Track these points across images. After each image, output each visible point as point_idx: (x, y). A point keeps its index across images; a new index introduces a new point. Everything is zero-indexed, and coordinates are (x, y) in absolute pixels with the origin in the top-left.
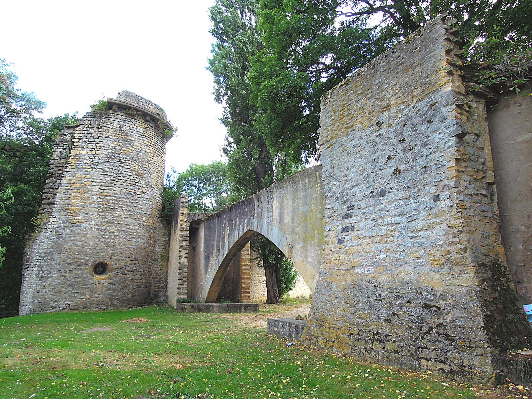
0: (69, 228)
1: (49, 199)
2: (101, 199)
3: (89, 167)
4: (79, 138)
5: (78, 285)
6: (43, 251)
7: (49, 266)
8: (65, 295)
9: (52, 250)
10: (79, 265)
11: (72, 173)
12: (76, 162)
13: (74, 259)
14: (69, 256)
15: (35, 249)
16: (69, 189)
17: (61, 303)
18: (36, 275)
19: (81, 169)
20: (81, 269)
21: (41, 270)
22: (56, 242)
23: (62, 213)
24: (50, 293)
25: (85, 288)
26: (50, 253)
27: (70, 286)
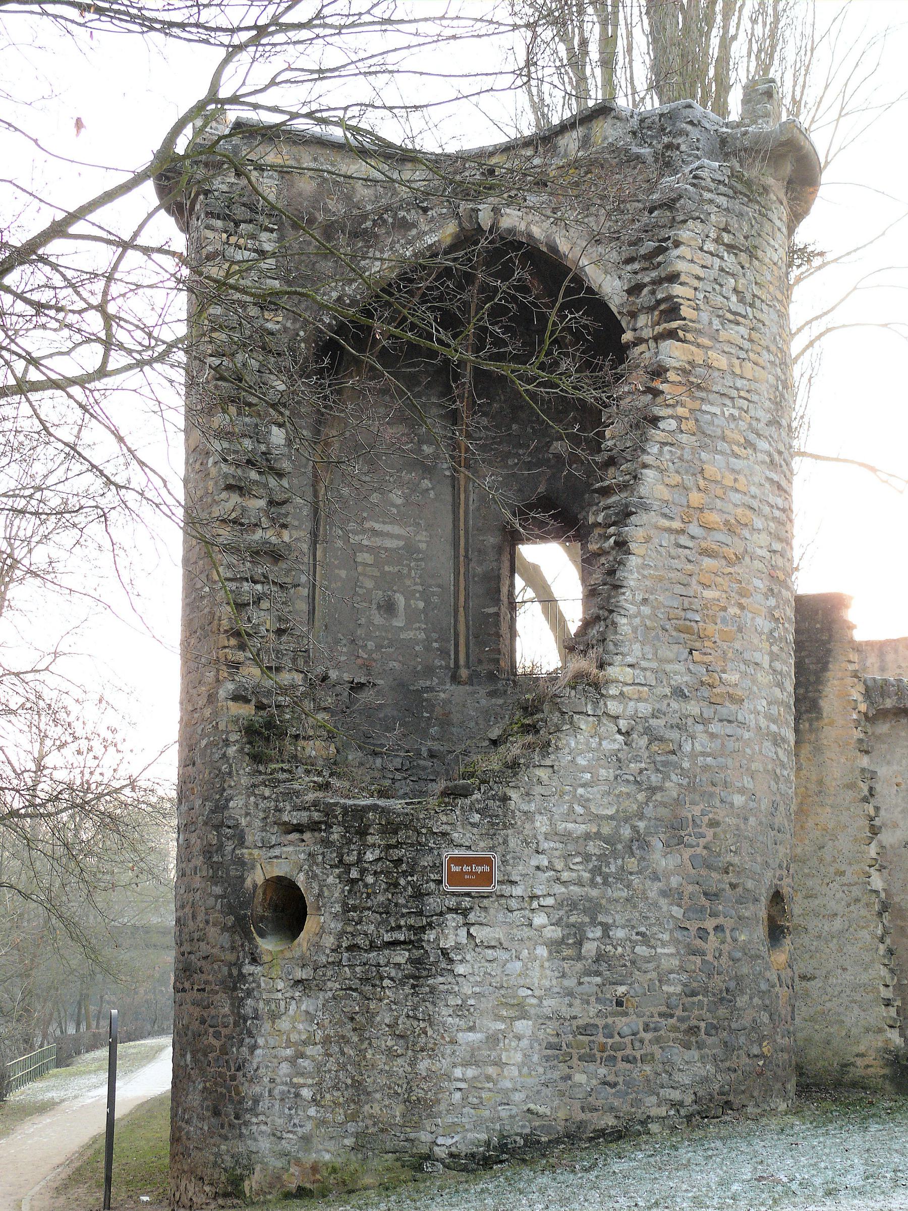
18: (555, 946)
21: (594, 922)
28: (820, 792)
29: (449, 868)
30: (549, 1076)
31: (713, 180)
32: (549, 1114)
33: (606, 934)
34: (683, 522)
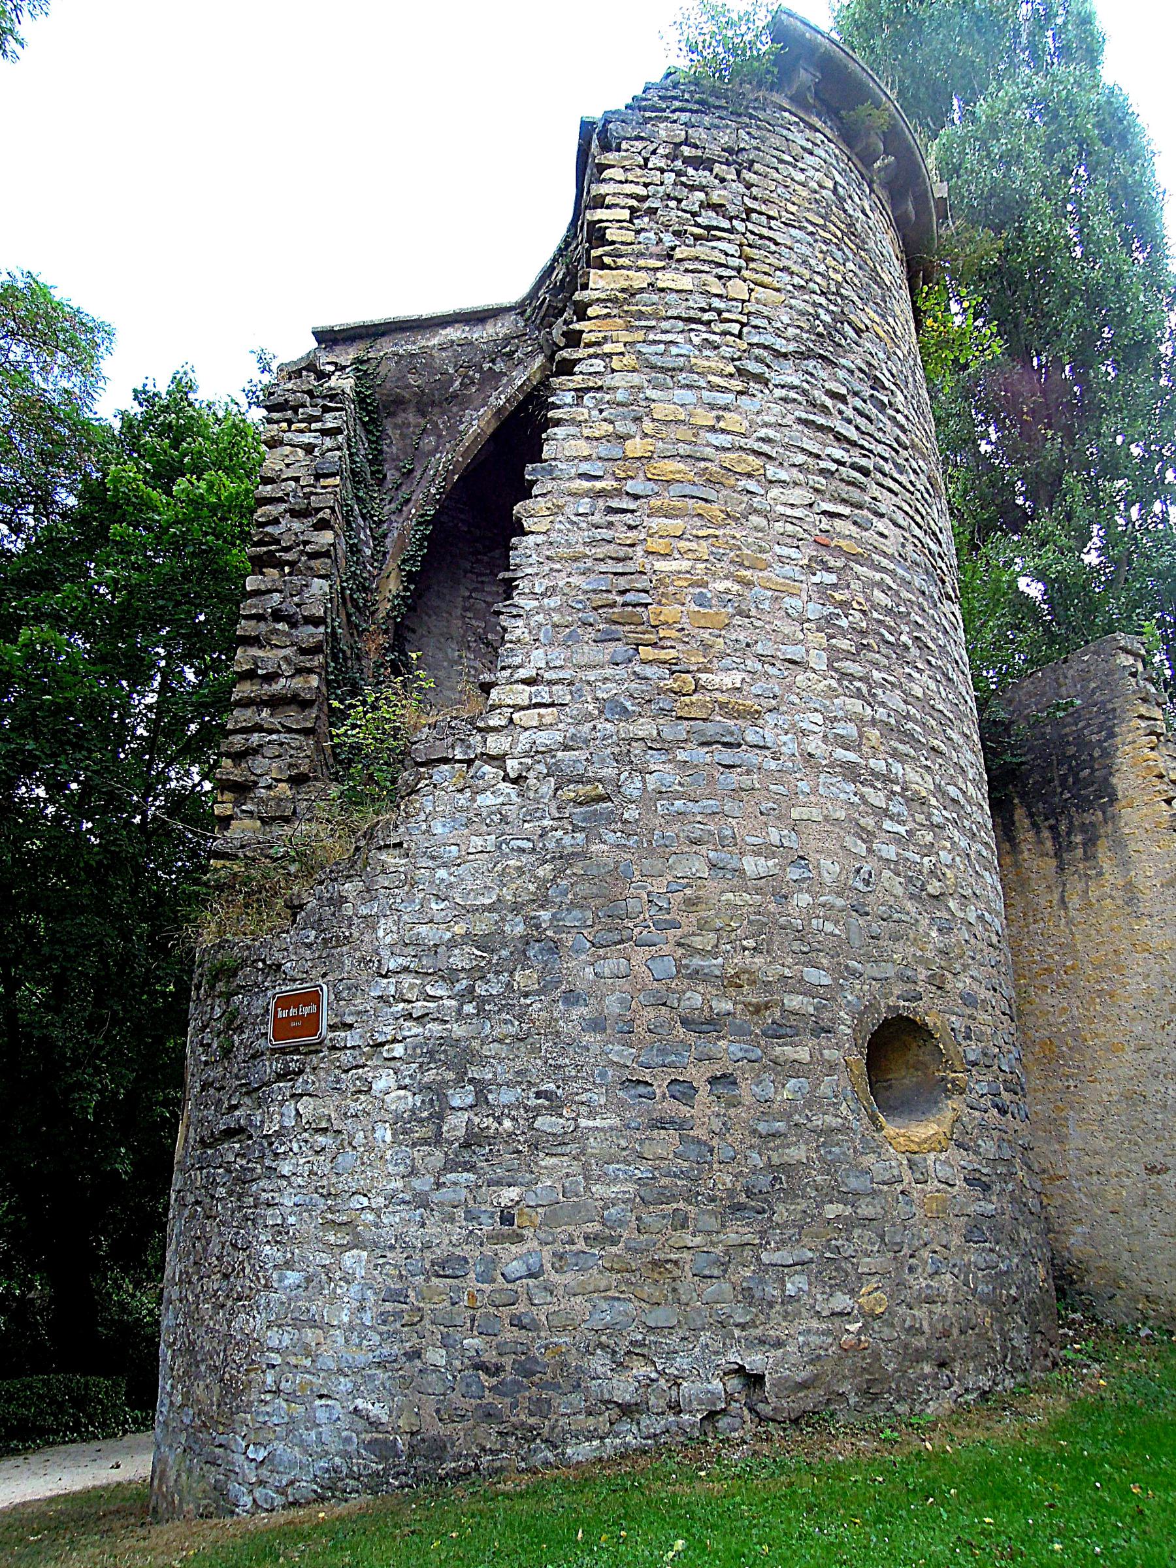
0: (664, 746)
1: (271, 678)
2: (829, 570)
3: (731, 369)
4: (634, 203)
5: (790, 1195)
6: (459, 929)
7: (535, 1050)
8: (711, 1289)
9: (545, 915)
10: (777, 1033)
11: (620, 396)
12: (639, 336)
13: (732, 982)
14: (697, 962)
15: (370, 922)
16: (618, 493)
17: (682, 1362)
18: (402, 1125)
19: (682, 377)
20: (795, 1069)
21: (460, 1079)
22: (566, 858)
23: (589, 652)
24: (568, 1278)
25: (848, 1225)
26: (526, 940)
27: (740, 1207)
28: (1131, 900)
29: (276, 1013)
30: (386, 1351)
31: (660, 98)
32: (385, 1419)
33: (481, 1100)
34: (618, 479)
